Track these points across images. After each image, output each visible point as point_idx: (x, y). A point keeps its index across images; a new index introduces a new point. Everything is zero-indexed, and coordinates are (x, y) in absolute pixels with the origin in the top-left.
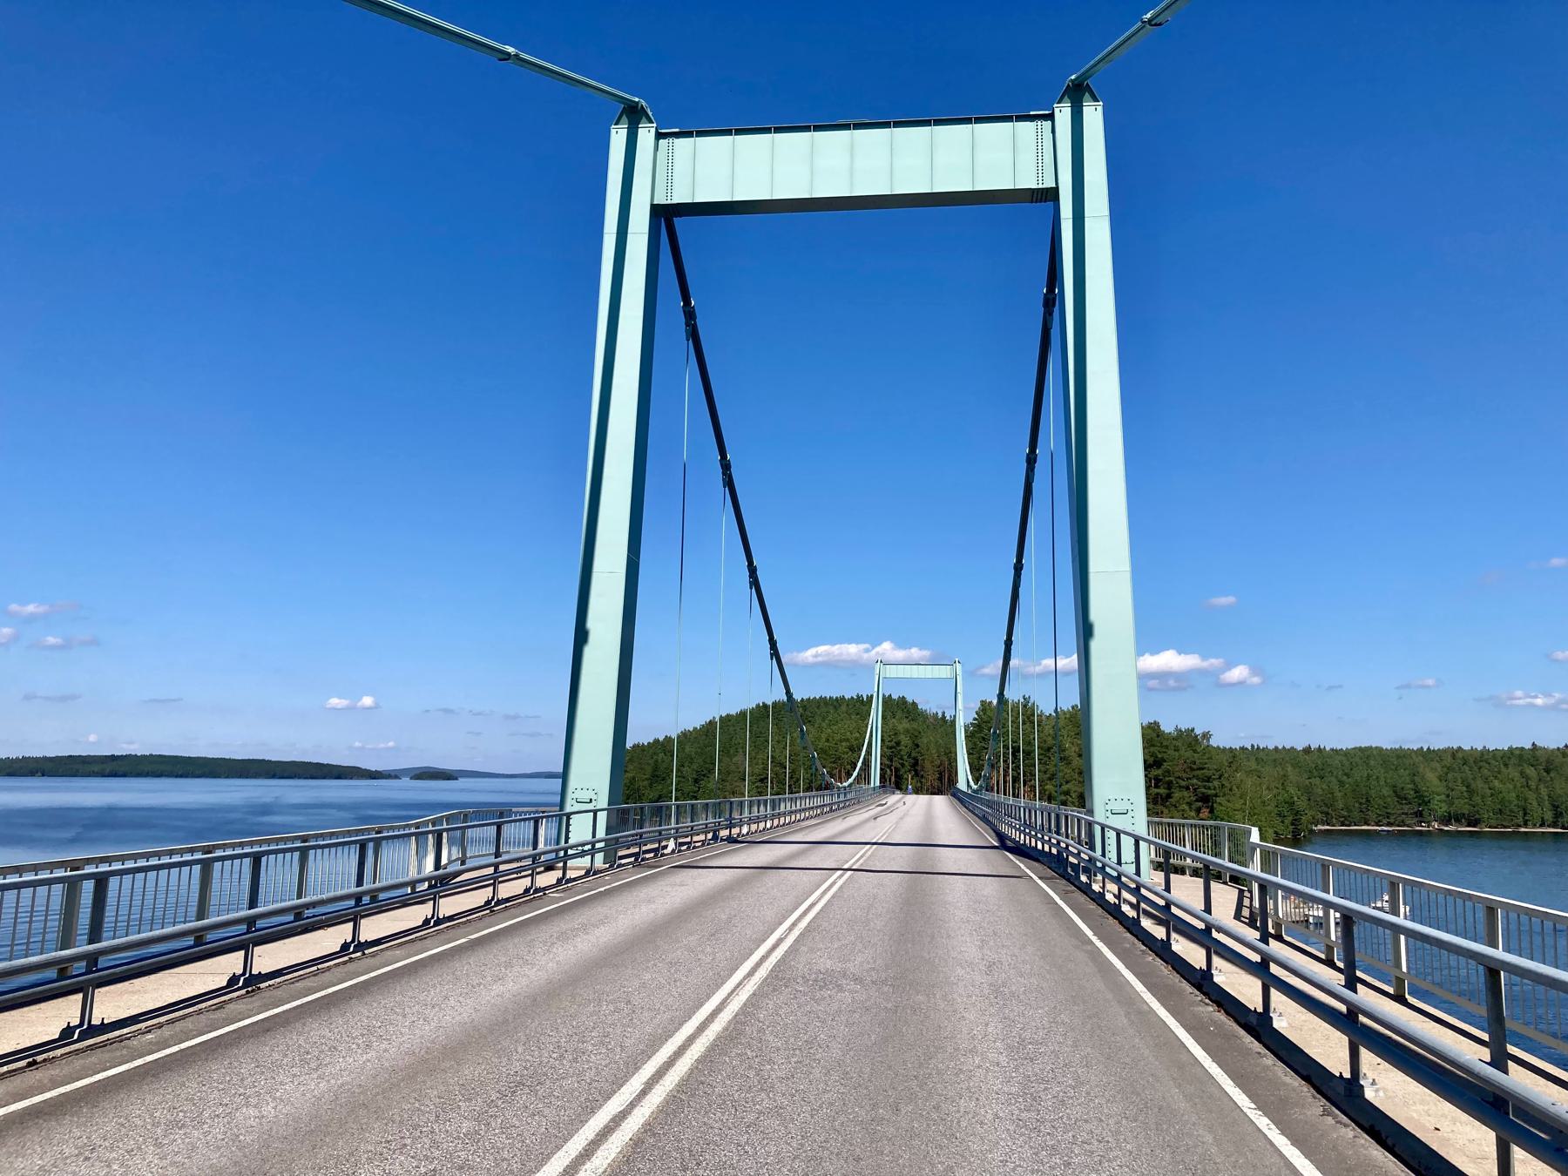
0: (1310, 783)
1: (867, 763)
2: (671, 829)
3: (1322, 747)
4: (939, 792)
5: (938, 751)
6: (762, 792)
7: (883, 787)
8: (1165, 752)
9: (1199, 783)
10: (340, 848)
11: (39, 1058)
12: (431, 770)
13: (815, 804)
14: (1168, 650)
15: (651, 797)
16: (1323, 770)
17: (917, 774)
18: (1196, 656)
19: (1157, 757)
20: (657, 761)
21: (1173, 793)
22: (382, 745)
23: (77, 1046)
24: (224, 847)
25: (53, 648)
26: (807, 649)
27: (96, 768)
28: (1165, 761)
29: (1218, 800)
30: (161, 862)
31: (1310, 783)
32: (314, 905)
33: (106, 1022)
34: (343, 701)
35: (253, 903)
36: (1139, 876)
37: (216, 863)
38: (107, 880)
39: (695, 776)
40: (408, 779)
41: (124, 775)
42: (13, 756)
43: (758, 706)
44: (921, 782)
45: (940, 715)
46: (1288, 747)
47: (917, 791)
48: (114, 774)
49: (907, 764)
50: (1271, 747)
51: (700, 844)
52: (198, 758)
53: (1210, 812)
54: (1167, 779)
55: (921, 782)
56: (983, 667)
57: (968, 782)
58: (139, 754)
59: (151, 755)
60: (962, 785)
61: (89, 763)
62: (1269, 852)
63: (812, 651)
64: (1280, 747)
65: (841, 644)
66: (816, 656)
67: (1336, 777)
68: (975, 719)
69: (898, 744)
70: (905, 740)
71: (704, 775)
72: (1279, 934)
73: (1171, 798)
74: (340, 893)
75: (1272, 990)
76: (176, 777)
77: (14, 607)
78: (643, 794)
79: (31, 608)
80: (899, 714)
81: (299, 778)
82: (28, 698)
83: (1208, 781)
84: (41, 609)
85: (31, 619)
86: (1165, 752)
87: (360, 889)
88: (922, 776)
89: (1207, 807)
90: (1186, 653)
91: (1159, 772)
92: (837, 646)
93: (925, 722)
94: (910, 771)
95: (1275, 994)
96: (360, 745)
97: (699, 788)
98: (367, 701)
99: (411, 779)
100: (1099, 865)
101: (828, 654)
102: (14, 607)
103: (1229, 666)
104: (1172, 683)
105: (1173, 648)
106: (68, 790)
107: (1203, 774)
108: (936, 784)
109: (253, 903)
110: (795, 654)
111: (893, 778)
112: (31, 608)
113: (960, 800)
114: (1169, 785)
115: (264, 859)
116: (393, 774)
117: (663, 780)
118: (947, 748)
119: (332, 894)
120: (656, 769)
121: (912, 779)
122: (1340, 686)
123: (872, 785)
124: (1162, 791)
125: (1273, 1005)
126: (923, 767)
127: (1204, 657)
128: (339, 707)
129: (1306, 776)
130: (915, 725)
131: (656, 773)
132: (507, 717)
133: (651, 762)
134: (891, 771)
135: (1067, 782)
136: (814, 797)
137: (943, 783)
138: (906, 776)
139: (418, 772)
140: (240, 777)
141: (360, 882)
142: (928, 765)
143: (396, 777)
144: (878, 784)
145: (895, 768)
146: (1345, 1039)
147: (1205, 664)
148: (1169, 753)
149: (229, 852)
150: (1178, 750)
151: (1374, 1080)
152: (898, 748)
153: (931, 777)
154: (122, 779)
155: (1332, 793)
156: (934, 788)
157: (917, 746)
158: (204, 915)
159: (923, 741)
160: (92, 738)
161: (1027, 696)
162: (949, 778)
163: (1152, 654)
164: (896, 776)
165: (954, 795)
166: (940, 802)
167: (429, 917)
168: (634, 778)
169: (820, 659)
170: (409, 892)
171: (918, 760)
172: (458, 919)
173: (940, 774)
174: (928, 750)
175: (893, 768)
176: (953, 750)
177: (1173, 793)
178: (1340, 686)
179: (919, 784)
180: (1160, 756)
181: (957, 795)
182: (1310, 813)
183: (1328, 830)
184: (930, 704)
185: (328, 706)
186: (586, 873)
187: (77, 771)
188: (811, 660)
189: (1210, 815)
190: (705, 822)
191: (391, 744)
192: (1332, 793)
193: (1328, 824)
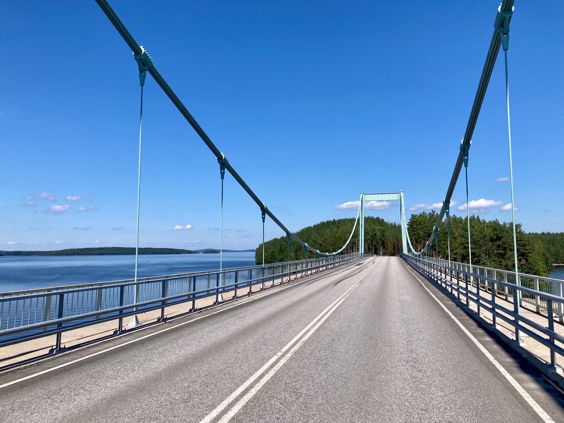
0: (548, 247)
1: (356, 235)
2: (133, 307)
3: (549, 232)
4: (393, 255)
5: (393, 238)
6: (310, 257)
7: (366, 253)
8: (502, 233)
9: (520, 247)
10: (177, 280)
11: (208, 309)
12: (210, 250)
13: (346, 259)
14: (482, 198)
15: (279, 258)
16: (553, 241)
17: (384, 247)
18: (493, 200)
19: (498, 236)
20: (281, 244)
21: (507, 252)
22: (194, 242)
23: (236, 300)
24: (106, 284)
25: (83, 211)
26: (343, 203)
27: (95, 252)
28: (503, 238)
29: (530, 255)
30: (79, 289)
31: (548, 247)
32: (170, 299)
33: (198, 308)
34: (180, 226)
35: (121, 304)
36: (441, 276)
37: (103, 289)
38: (195, 277)
39: (295, 250)
40: (202, 253)
41: (104, 254)
42: (68, 248)
43: (321, 223)
44: (386, 251)
45: (393, 224)
46: (534, 233)
47: (384, 254)
48: (101, 254)
49: (379, 243)
50: (539, 232)
51: (300, 278)
52: (92, 248)
53: (526, 261)
54: (504, 246)
55: (386, 251)
56: (410, 207)
57: (342, 253)
58: (109, 247)
59: (113, 247)
60: (405, 251)
61: (92, 250)
62: (526, 277)
63: (346, 204)
64: (531, 233)
65: (356, 201)
66: (347, 206)
67: (560, 244)
68: (409, 223)
69: (375, 235)
70: (378, 233)
71: (299, 250)
72: (561, 321)
73: (507, 255)
74: (202, 290)
75: (480, 307)
76: (122, 254)
77: (69, 198)
78: (277, 257)
79: (74, 198)
80: (377, 224)
81: (164, 254)
82: (76, 228)
83: (524, 247)
84: (78, 198)
85: (74, 202)
86: (502, 233)
87: (194, 292)
88: (387, 248)
89: (524, 259)
90: (488, 200)
91: (500, 242)
92: (355, 202)
93: (387, 227)
94: (381, 246)
95: (481, 308)
96: (187, 242)
97: (297, 254)
98: (189, 226)
99: (203, 253)
100: (425, 270)
101: (351, 205)
102: (69, 198)
103: (505, 204)
104: (482, 211)
105: (483, 198)
106: (88, 260)
107: (522, 243)
108: (392, 251)
109: (121, 304)
110: (339, 205)
111: (373, 250)
112: (74, 198)
113: (406, 260)
114: (505, 249)
115: (196, 278)
116: (196, 252)
117: (284, 252)
118: (397, 237)
119: (200, 291)
120: (281, 247)
121: (382, 249)
122: (550, 210)
123: (360, 252)
124: (502, 252)
125: (480, 312)
126: (387, 244)
127: (495, 201)
128: (179, 229)
129: (546, 244)
130: (383, 228)
131: (281, 249)
132: (237, 231)
133: (280, 245)
134: (372, 246)
135: (456, 249)
136: (347, 256)
137: (396, 251)
138: (379, 248)
139: (205, 251)
140: (143, 254)
141: (218, 285)
142: (389, 244)
143: (198, 253)
144: (363, 252)
145: (374, 245)
146: (549, 349)
147: (496, 203)
148: (504, 233)
149: (228, 271)
150: (508, 233)
151: (523, 340)
152: (375, 236)
153: (390, 248)
154: (102, 256)
155: (558, 251)
156: (391, 253)
157: (384, 236)
158: (164, 296)
159: (387, 234)
160: (97, 242)
161: (434, 210)
162: (398, 249)
163: (476, 200)
164: (375, 248)
165: (401, 257)
166: (394, 260)
167: (215, 302)
168: (273, 251)
169: (348, 207)
170: (135, 310)
171: (384, 242)
172: (175, 318)
173: (394, 247)
174: (388, 237)
175: (373, 245)
176: (399, 237)
177: (507, 252)
178: (550, 210)
179: (385, 251)
180: (500, 235)
181: (402, 256)
182: (551, 259)
183: (556, 266)
184: (389, 218)
185: (175, 228)
186: (189, 312)
187: (89, 253)
188: (345, 207)
189: (526, 263)
190: (119, 307)
191: (197, 241)
192: (558, 251)
193: (557, 263)
